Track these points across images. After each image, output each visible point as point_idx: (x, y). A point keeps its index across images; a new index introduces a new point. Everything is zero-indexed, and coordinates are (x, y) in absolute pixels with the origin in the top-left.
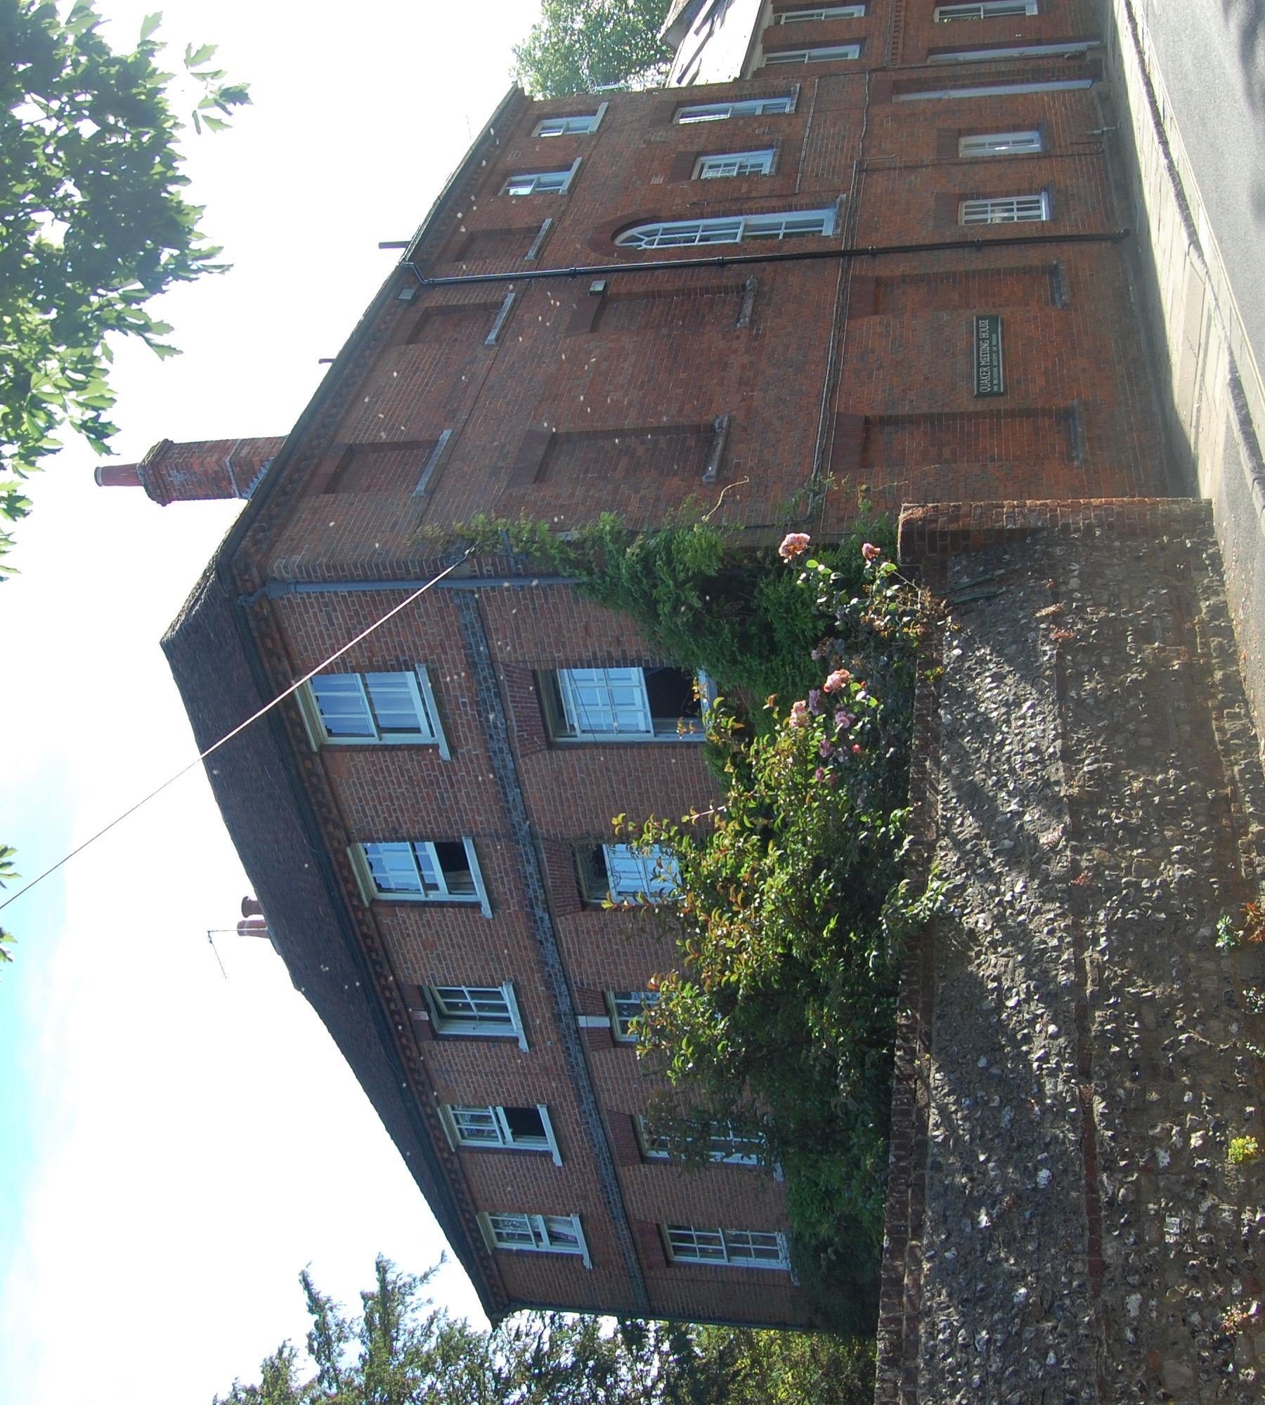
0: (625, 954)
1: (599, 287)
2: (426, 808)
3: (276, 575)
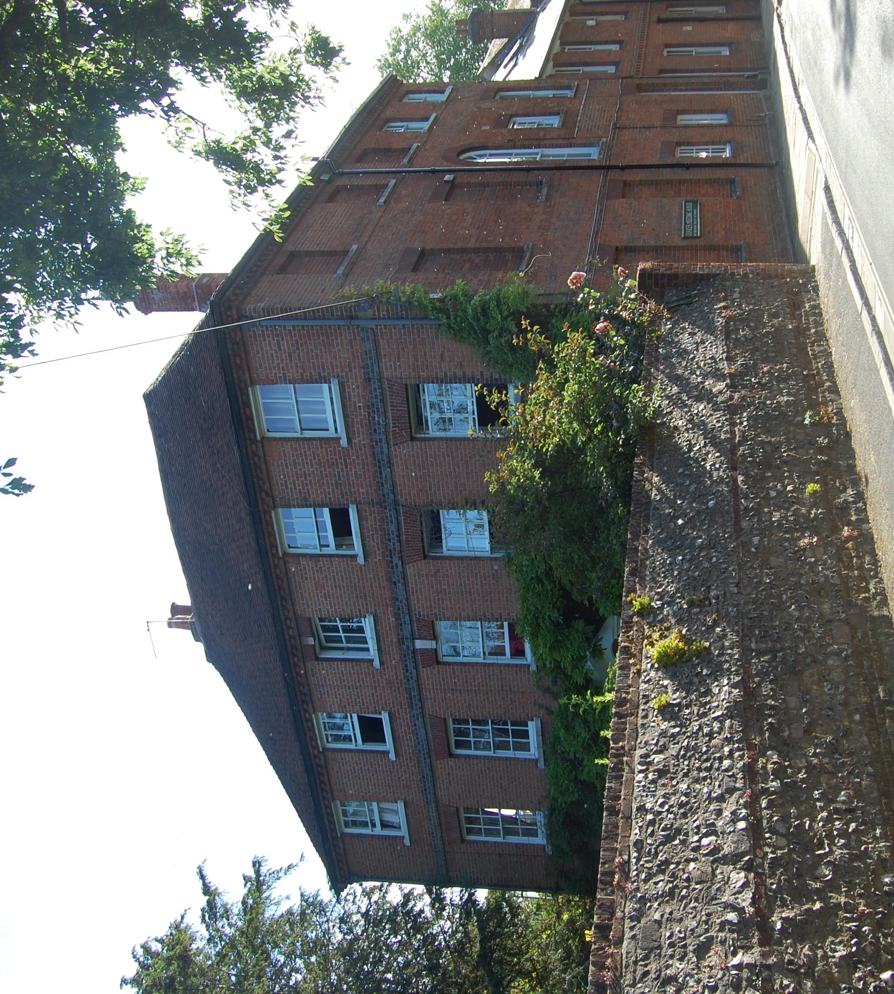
0: (450, 593)
1: (448, 177)
2: (328, 483)
3: (248, 314)
